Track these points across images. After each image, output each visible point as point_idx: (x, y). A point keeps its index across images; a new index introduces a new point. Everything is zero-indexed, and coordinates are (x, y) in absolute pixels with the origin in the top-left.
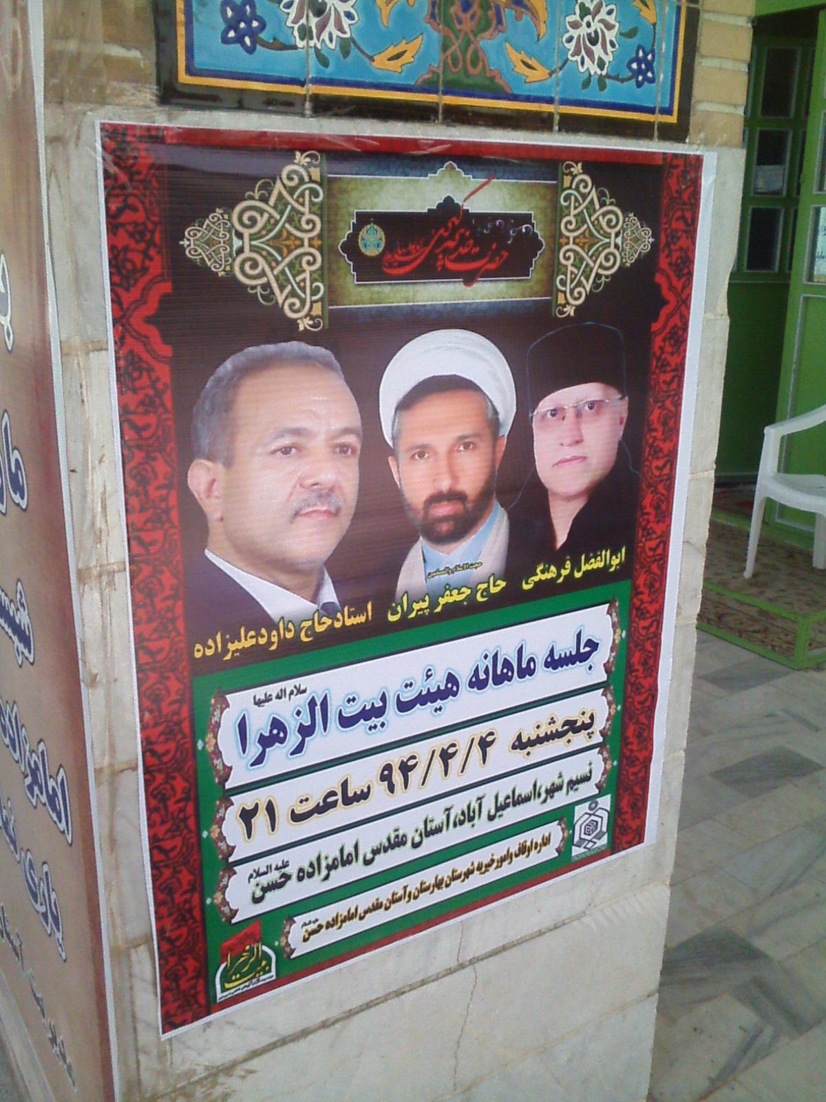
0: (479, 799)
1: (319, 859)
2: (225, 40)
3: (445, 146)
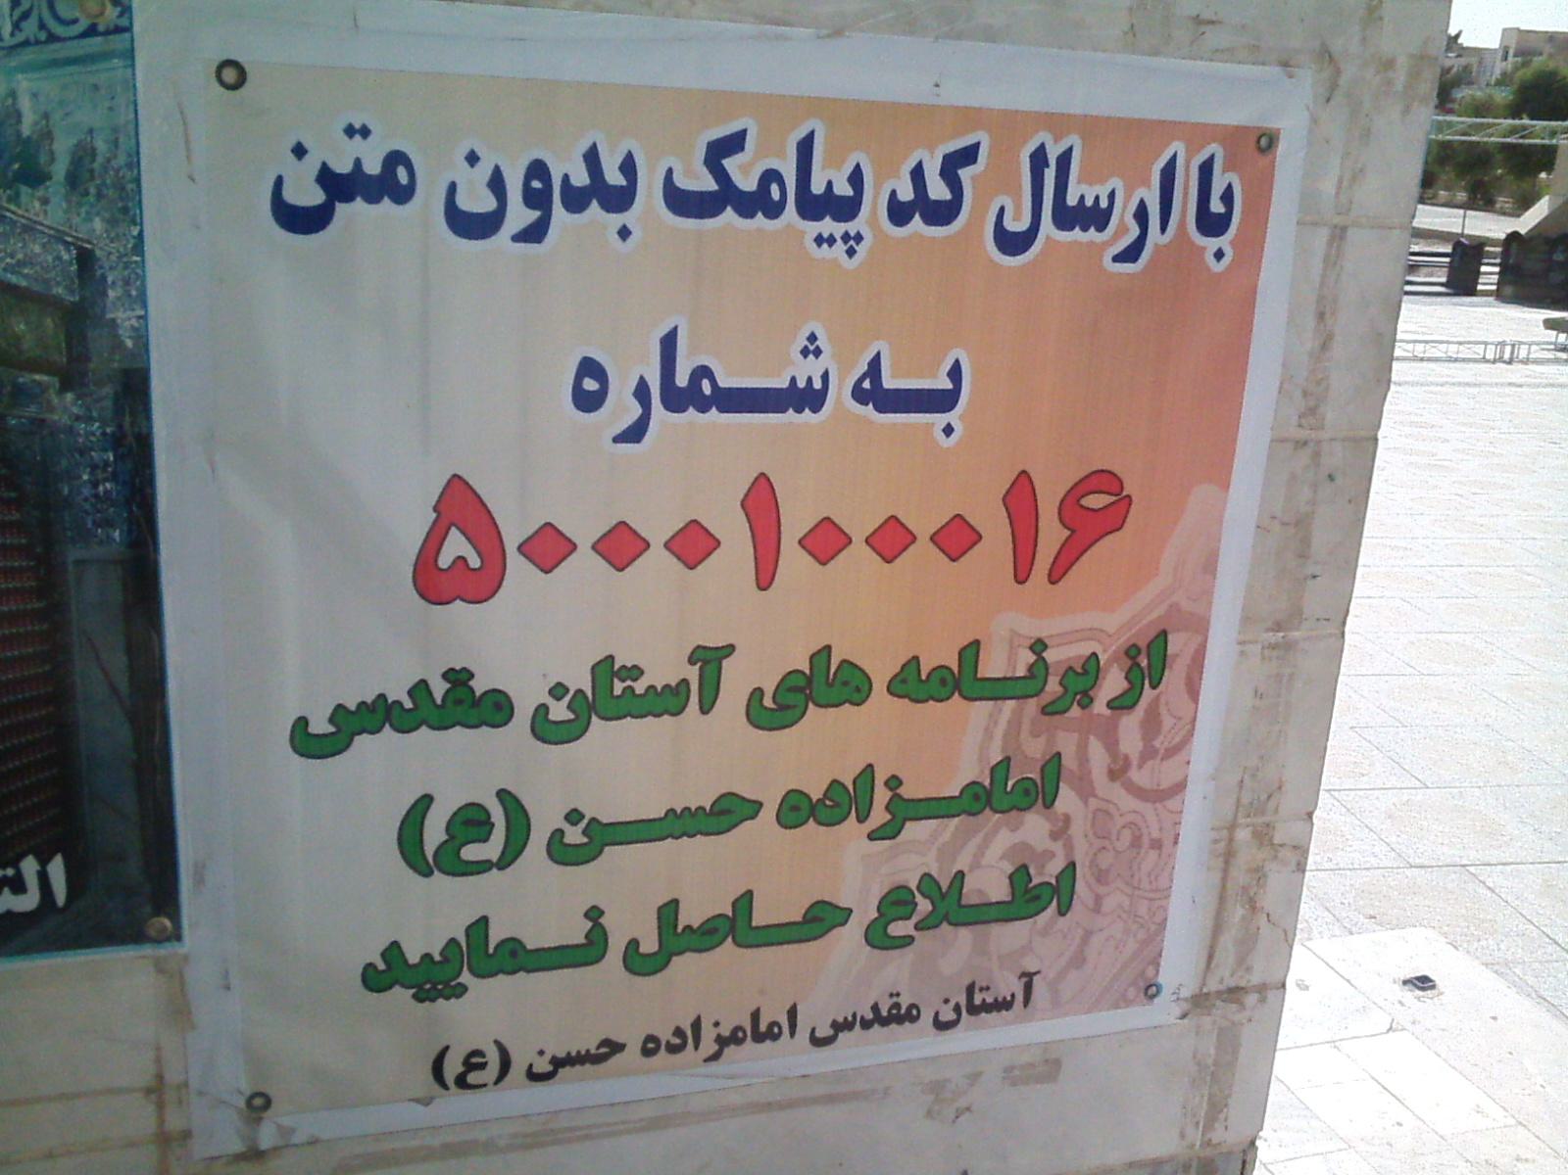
1: (696, 1025)
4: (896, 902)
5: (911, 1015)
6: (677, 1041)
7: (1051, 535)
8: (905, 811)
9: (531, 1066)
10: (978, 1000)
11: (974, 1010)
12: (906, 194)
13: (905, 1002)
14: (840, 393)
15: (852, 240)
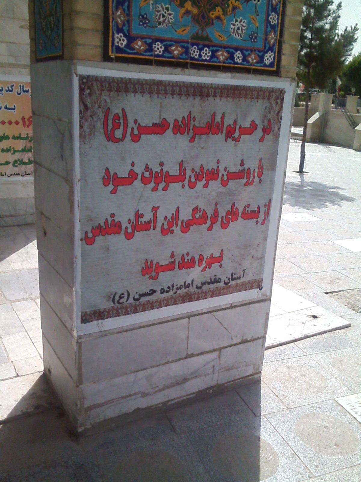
0: (244, 270)
1: (173, 286)
2: (139, 25)
3: (278, 11)
4: (16, 162)
5: (19, 174)
6: (168, 290)
7: (27, 123)
8: (15, 151)
9: (134, 296)
10: (234, 277)
11: (26, 174)
12: (7, 89)
13: (18, 173)
14: (3, 108)
15: (2, 94)
